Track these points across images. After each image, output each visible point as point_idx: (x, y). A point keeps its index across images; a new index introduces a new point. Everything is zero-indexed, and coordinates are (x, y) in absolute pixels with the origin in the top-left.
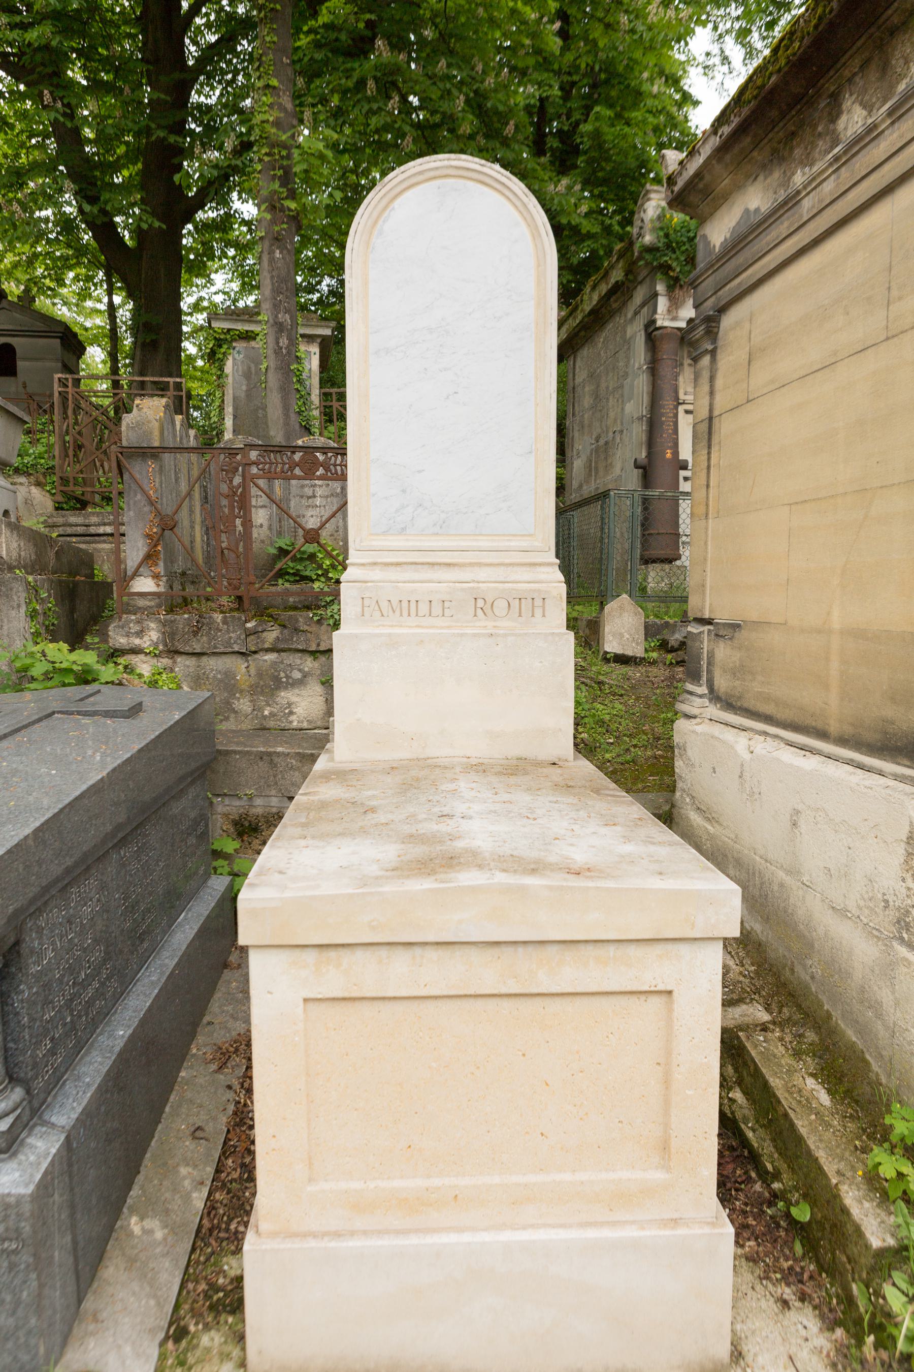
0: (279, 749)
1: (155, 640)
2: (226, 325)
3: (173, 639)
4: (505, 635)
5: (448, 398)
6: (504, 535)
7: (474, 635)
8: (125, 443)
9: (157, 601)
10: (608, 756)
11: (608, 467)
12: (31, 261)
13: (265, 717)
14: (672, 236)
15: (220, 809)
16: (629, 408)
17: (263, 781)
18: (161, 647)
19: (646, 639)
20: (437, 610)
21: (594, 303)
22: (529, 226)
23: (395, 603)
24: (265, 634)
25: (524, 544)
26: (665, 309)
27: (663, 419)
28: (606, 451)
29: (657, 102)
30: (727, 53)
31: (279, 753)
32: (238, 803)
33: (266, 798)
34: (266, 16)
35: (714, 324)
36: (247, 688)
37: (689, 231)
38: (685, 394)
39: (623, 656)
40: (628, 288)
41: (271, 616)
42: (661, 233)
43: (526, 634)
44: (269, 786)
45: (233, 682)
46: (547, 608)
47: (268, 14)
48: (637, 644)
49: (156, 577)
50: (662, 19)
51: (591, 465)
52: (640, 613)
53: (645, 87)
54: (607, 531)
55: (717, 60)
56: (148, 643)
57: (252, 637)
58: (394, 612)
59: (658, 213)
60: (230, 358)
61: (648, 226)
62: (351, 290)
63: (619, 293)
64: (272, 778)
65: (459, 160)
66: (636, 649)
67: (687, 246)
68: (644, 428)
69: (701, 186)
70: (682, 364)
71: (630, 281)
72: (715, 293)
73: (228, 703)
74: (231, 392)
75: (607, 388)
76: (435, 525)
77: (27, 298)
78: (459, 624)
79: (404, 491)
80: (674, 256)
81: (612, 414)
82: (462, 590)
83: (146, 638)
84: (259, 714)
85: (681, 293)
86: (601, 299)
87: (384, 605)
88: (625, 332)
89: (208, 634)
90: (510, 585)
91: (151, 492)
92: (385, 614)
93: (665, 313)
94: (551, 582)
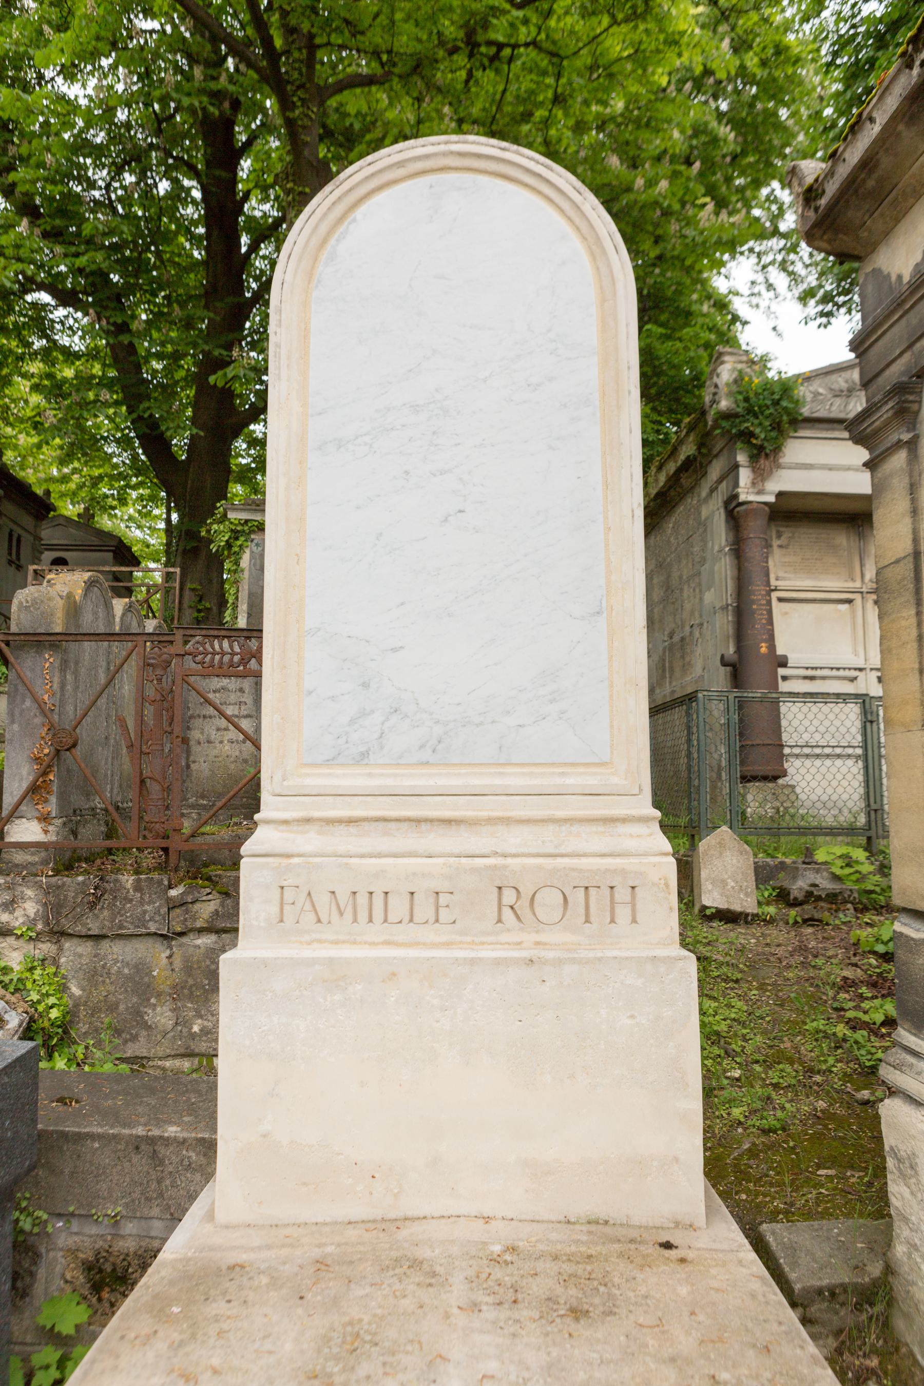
0: (172, 1130)
1: (32, 915)
2: (244, 516)
3: (59, 913)
4: (559, 962)
5: (446, 520)
6: (553, 764)
7: (498, 962)
8: (14, 629)
9: (43, 854)
10: (737, 1112)
11: (686, 667)
12: (96, 481)
13: (193, 1036)
14: (753, 400)
15: (62, 1241)
16: (709, 597)
17: (138, 1190)
18: (40, 926)
19: (758, 888)
20: (425, 911)
21: (661, 484)
22: (585, 239)
23: (343, 897)
24: (197, 906)
25: (592, 781)
26: (749, 481)
27: (755, 607)
28: (682, 648)
29: (707, 320)
30: (771, 281)
31: (168, 1139)
32: (94, 1230)
33: (143, 1222)
34: (294, 199)
35: (911, 398)
36: (167, 990)
37: (773, 393)
38: (777, 579)
39: (728, 911)
40: (701, 464)
41: (209, 879)
42: (740, 397)
43: (600, 959)
44: (148, 1199)
45: (146, 979)
46: (639, 906)
47: (297, 198)
48: (747, 894)
49: (44, 819)
50: (713, 225)
51: (664, 665)
52: (747, 853)
53: (695, 307)
54: (695, 743)
55: (762, 288)
56: (21, 920)
57: (178, 911)
58: (341, 914)
59: (734, 376)
60: (248, 551)
61: (723, 390)
62: (278, 346)
63: (691, 470)
64: (154, 1185)
65: (466, 142)
66: (746, 902)
67: (772, 410)
68: (730, 618)
69: (871, 183)
70: (771, 546)
71: (704, 455)
72: (910, 346)
73: (138, 1013)
74: (246, 587)
75: (681, 577)
76: (422, 746)
77: (87, 516)
78: (469, 939)
79: (365, 685)
80: (756, 422)
81: (688, 606)
82: (475, 870)
83: (19, 913)
84: (185, 1030)
85: (767, 463)
86: (669, 479)
87: (323, 901)
88: (700, 513)
89: (112, 906)
90: (566, 860)
91: (46, 697)
92: (324, 917)
93: (749, 485)
94: (645, 854)
